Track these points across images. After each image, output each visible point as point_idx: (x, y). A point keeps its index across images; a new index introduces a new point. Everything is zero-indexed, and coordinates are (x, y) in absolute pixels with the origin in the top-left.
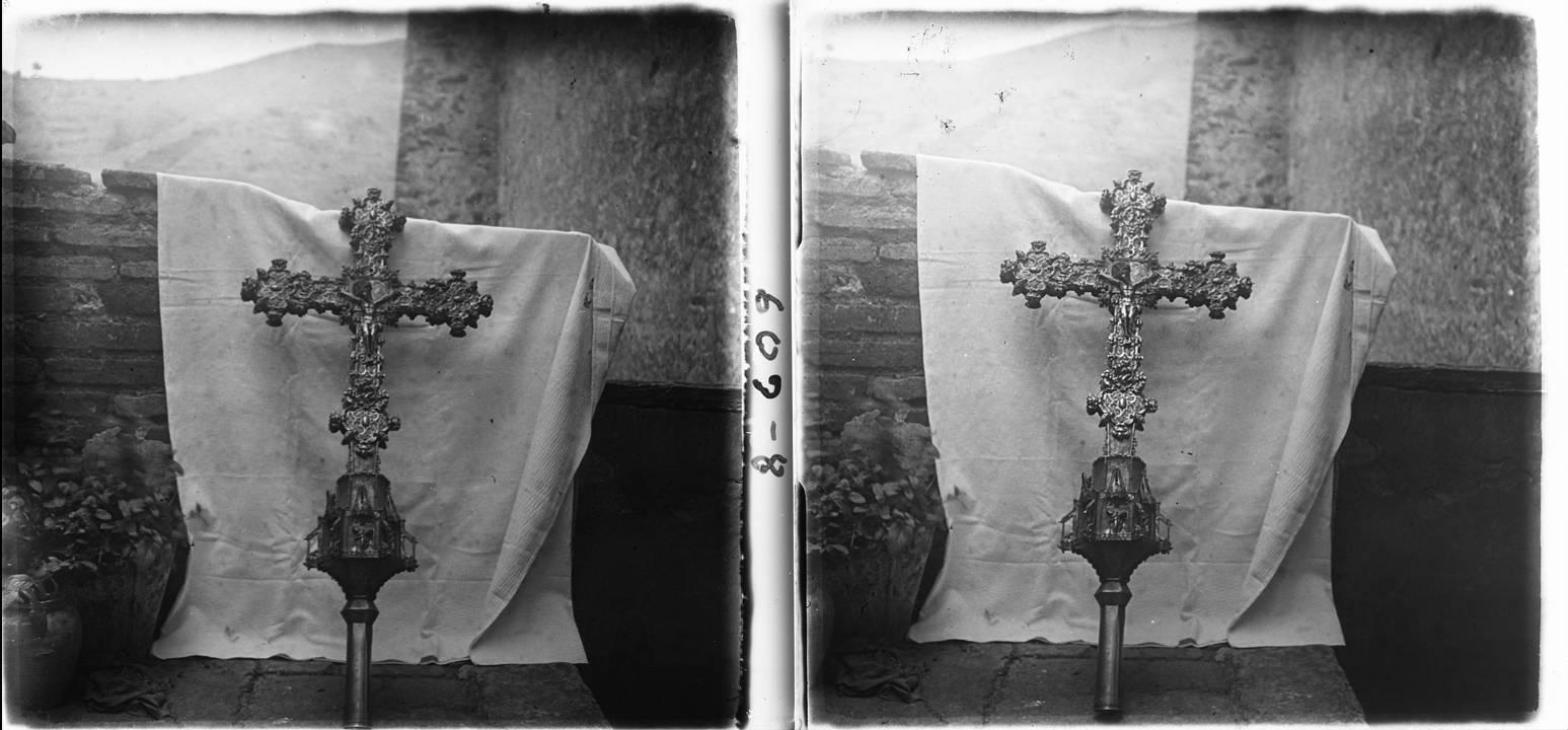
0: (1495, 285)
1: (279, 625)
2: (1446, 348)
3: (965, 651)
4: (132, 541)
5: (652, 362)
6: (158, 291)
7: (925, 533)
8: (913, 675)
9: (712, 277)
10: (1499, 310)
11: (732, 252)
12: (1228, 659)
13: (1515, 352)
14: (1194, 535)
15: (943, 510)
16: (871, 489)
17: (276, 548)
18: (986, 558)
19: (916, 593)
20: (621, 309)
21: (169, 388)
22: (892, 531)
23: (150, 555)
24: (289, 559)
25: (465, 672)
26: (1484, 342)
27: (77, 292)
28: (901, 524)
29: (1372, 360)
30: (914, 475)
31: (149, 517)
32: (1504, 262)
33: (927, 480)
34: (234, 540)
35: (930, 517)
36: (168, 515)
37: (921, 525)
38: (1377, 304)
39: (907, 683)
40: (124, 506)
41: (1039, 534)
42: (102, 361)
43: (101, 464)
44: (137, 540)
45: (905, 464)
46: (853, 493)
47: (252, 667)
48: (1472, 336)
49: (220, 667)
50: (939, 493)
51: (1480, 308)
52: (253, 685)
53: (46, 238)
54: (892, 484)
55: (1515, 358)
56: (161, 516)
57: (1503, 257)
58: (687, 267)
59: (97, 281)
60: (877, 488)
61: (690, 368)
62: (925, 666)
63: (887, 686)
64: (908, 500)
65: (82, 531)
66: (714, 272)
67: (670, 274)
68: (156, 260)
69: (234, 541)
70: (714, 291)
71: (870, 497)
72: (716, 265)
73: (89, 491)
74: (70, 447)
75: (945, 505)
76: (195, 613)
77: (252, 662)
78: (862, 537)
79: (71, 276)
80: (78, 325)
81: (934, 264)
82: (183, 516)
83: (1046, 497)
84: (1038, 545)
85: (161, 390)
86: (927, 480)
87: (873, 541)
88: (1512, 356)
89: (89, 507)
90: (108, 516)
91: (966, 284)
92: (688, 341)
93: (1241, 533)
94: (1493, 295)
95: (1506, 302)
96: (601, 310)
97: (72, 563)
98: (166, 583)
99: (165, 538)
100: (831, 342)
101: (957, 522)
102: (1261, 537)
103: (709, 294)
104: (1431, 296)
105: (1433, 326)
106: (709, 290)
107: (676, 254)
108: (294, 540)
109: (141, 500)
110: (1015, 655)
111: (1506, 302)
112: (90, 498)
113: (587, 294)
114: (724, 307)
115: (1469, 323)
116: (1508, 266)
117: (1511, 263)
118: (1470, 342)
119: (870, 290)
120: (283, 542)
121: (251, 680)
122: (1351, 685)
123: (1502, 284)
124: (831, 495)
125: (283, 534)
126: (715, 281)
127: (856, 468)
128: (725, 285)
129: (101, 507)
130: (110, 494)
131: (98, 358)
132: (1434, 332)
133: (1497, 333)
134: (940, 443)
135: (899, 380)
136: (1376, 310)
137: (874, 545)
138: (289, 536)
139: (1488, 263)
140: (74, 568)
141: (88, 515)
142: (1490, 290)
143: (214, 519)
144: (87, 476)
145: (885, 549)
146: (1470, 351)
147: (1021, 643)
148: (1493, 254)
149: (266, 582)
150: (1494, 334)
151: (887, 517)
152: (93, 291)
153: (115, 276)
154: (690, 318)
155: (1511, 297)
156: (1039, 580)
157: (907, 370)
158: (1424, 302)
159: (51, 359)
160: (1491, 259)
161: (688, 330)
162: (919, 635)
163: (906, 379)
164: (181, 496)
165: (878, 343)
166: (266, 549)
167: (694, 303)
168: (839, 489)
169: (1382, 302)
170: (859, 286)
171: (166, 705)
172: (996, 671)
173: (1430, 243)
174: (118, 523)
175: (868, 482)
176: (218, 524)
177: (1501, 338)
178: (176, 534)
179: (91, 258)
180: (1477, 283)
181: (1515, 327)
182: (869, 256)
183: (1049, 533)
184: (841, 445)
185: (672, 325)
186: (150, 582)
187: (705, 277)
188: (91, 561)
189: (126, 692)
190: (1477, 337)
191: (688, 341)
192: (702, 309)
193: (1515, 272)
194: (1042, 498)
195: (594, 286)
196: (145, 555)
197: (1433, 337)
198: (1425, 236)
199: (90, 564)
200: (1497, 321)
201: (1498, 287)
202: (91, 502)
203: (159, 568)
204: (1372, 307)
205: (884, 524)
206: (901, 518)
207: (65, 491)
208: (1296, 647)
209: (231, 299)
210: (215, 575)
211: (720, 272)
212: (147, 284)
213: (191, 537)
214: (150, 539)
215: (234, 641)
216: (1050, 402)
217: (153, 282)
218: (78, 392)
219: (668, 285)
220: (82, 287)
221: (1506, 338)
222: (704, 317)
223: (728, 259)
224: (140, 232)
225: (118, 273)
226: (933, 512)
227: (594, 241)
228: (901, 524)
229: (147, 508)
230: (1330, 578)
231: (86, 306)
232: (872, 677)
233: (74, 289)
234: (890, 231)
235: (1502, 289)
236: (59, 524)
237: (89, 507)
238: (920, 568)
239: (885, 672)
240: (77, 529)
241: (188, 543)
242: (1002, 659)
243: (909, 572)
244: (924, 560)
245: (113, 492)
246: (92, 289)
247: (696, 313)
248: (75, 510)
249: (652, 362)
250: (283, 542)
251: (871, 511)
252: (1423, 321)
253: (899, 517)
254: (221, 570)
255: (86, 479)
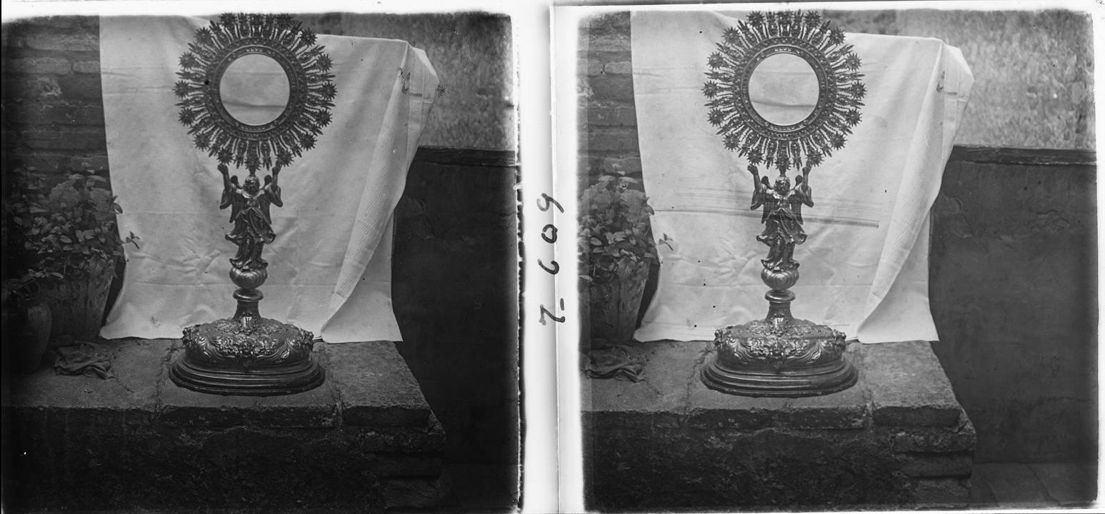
0: (1043, 91)
1: (188, 316)
2: (1009, 136)
3: (674, 347)
4: (615, 260)
5: (449, 135)
6: (100, 83)
7: (644, 265)
8: (638, 363)
9: (493, 75)
10: (1046, 108)
11: (507, 56)
12: (321, 350)
13: (1058, 138)
14: (295, 266)
15: (656, 250)
16: (605, 236)
17: (186, 263)
18: (151, 282)
19: (638, 308)
20: (964, 93)
21: (110, 152)
22: (92, 262)
23: (99, 268)
24: (194, 270)
25: (317, 347)
26: (1036, 132)
27: (44, 84)
28: (628, 260)
29: (956, 143)
30: (635, 227)
31: (98, 242)
32: (1050, 74)
33: (644, 229)
34: (157, 258)
35: (647, 255)
36: (111, 240)
37: (641, 260)
38: (961, 102)
39: (634, 369)
40: (81, 235)
41: (188, 265)
42: (61, 132)
43: (63, 205)
44: (89, 257)
45: (99, 218)
46: (63, 236)
47: (169, 344)
48: (1027, 127)
49: (682, 347)
50: (653, 239)
51: (483, 110)
52: (704, 358)
53: (20, 44)
54: (621, 233)
55: (1057, 143)
56: (106, 241)
57: (1050, 70)
58: (475, 67)
59: (58, 75)
60: (609, 236)
61: (1026, 137)
62: (646, 357)
63: (620, 371)
64: (632, 244)
65: (50, 251)
66: (494, 72)
67: (463, 72)
68: (99, 61)
69: (157, 258)
70: (494, 84)
71: (75, 241)
72: (496, 66)
73: (56, 222)
74: (41, 193)
75: (657, 247)
76: (130, 308)
77: (169, 341)
78: (600, 269)
79: (38, 71)
80: (44, 107)
81: (112, 76)
82: (655, 244)
83: (192, 239)
84: (188, 272)
85: (104, 152)
86: (644, 229)
87: (608, 272)
88: (1055, 141)
89: (56, 234)
90: (69, 241)
91: (134, 90)
92: (475, 121)
93: (327, 264)
94: (1042, 98)
95: (1052, 103)
96: (950, 94)
97: (44, 273)
98: (643, 289)
99: (109, 256)
100: (40, 131)
101: (132, 257)
102: (343, 268)
103: (1040, 85)
104: (998, 99)
105: (999, 121)
106: (490, 84)
107: (468, 58)
108: (734, 259)
109: (92, 231)
110: (709, 349)
111: (1052, 103)
112: (56, 228)
113: (939, 82)
114: (500, 96)
115: (1025, 118)
116: (1053, 77)
117: (1055, 74)
118: (475, 134)
119: (66, 95)
120: (191, 259)
121: (169, 353)
122: (410, 367)
123: (1049, 89)
124: (48, 237)
125: (191, 253)
126: (495, 77)
127: (64, 219)
128: (502, 80)
129: (64, 234)
130: (70, 226)
131: (59, 130)
132: (1000, 125)
133: (1045, 126)
134: (652, 203)
135: (623, 159)
136: (961, 107)
137: (609, 275)
138: (194, 254)
139: (1039, 75)
140: (45, 277)
141: (56, 239)
142: (1040, 94)
143: (143, 244)
144: (54, 213)
145: (617, 277)
146: (1026, 137)
147: (177, 339)
148: (1043, 69)
149: (716, 288)
150: (1043, 126)
151: (617, 255)
152: (54, 83)
153: (70, 72)
154: (1026, 102)
155: (1055, 100)
156: (188, 298)
157: (626, 152)
158: (993, 104)
159: (26, 132)
160: (1042, 72)
161: (474, 112)
162: (640, 336)
163: (627, 159)
164: (119, 226)
165: (73, 132)
166: (178, 263)
167: (479, 94)
168: (52, 234)
169: (966, 101)
170: (59, 91)
171: (642, 373)
172: (696, 360)
173: (447, 63)
174: (77, 247)
175: (603, 231)
176: (145, 248)
177: (1048, 129)
178: (116, 253)
179: (53, 59)
180: (481, 92)
181: (1058, 120)
182: (65, 70)
183: (195, 264)
184: (49, 203)
185: (1014, 107)
186: (631, 288)
187: (488, 74)
188: (58, 271)
189: (613, 364)
190: (480, 130)
191: (475, 121)
192: (1035, 95)
193: (1058, 81)
194: (190, 240)
195: (945, 76)
196: (95, 267)
197: (448, 130)
198: (443, 59)
199: (58, 274)
200: (1045, 117)
201: (1046, 93)
202: (57, 231)
203: (104, 277)
204: (958, 105)
205: (615, 260)
206: (627, 256)
207: (40, 223)
208: (369, 342)
209: (152, 88)
210: (678, 284)
211: (499, 71)
212: (93, 77)
213: (127, 256)
214: (98, 256)
215: (157, 327)
216: (729, 173)
217: (97, 76)
218: (45, 155)
219: (1012, 78)
220: (46, 80)
221: (1051, 128)
222: (1036, 101)
223: (504, 61)
224: (87, 40)
225: (72, 70)
226: (649, 252)
227: (411, 46)
228: (628, 260)
229: (96, 237)
230: (390, 296)
231: (49, 93)
232: (610, 365)
233: (41, 82)
234: (79, 52)
235: (1049, 93)
236: (35, 245)
237: (56, 234)
238: (641, 291)
239: (619, 362)
240: (46, 250)
241: (124, 260)
242: (700, 352)
243: (632, 293)
244: (643, 285)
245: (73, 225)
246: (53, 82)
247: (1030, 98)
248: (46, 237)
249: (449, 135)
250: (191, 259)
251: (75, 249)
252: (440, 119)
253: (625, 255)
254: (683, 280)
255: (53, 216)
